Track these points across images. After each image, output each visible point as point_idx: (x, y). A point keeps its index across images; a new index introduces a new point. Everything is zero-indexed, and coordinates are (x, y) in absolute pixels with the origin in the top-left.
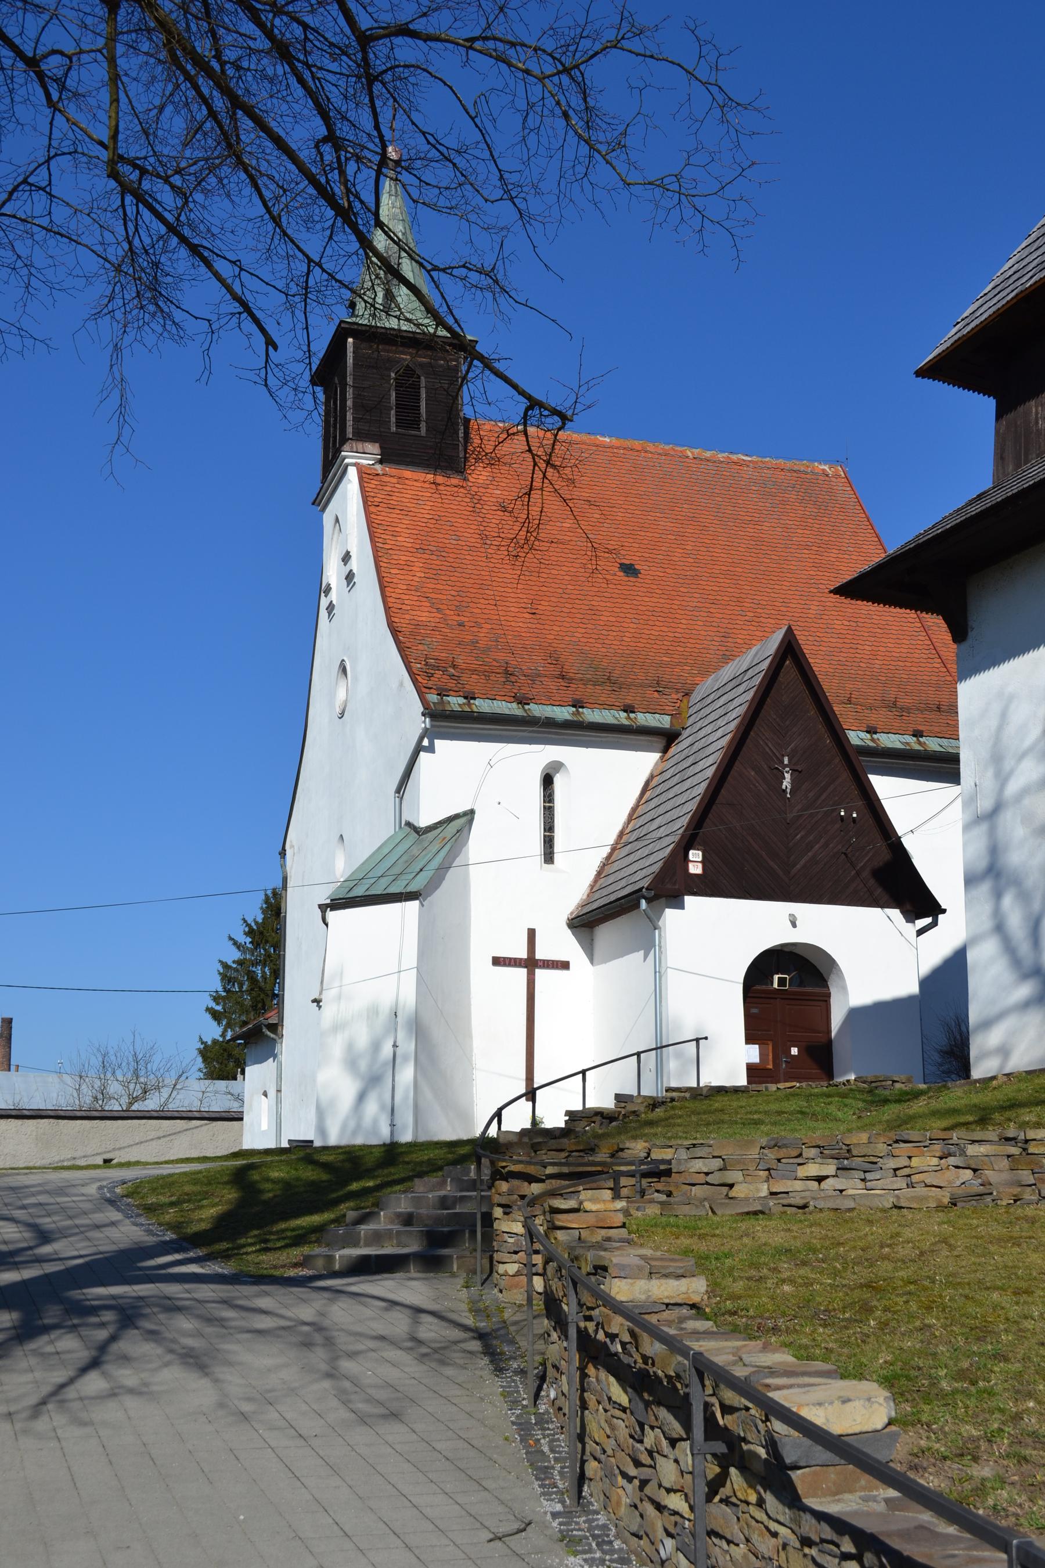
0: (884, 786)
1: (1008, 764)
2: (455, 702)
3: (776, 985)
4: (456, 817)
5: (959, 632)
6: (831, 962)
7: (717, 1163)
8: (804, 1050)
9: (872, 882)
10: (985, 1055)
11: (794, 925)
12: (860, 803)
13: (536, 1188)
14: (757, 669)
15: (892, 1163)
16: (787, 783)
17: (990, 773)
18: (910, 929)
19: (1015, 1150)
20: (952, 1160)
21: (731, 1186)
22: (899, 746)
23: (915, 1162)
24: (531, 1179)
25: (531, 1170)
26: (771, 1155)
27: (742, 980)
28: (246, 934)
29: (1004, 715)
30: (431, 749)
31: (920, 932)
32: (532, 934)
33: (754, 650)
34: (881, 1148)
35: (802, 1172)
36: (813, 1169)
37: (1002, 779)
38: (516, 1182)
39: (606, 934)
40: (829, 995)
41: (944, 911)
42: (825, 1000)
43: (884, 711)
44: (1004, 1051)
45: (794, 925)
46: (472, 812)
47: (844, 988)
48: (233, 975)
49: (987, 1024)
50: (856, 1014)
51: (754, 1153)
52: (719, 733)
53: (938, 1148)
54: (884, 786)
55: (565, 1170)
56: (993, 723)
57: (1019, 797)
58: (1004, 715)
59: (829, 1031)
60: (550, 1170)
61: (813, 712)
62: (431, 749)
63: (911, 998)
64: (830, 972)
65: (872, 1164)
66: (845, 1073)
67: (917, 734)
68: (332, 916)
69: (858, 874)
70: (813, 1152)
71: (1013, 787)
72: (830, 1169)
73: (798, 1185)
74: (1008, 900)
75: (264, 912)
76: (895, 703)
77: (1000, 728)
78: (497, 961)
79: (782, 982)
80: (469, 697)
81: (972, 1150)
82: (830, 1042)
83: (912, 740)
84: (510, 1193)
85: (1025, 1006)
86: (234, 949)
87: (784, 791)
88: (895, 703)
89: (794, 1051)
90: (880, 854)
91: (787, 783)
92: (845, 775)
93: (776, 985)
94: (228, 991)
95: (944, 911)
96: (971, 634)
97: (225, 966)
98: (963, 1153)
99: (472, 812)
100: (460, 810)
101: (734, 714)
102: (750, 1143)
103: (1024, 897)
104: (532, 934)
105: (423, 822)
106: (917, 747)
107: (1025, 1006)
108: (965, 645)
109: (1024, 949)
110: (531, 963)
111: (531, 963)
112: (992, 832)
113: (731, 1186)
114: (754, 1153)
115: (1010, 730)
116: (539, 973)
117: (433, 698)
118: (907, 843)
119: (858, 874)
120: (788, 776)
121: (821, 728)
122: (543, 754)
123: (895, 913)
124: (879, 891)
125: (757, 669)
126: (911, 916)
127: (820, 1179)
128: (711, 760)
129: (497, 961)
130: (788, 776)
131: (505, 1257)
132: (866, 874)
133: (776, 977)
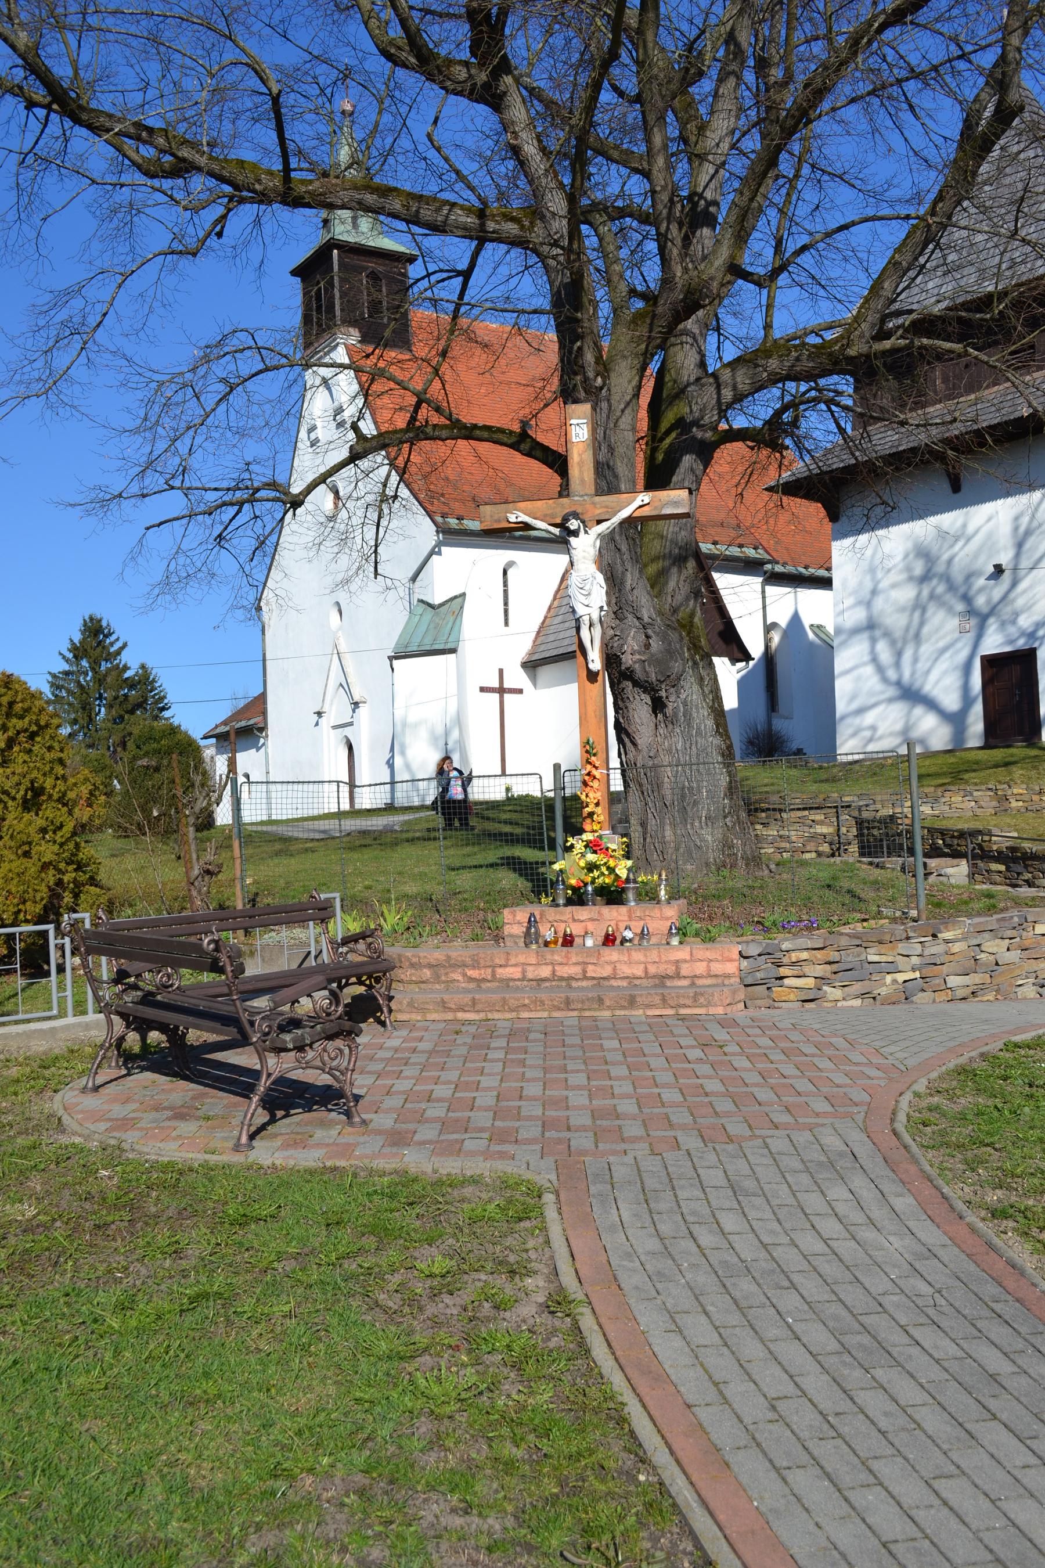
0: (723, 581)
2: (453, 522)
4: (456, 597)
5: (834, 516)
28: (70, 651)
30: (439, 553)
32: (501, 671)
39: (544, 672)
46: (463, 595)
48: (61, 683)
53: (962, 793)
62: (439, 553)
68: (395, 662)
75: (83, 633)
78: (482, 689)
80: (460, 518)
81: (975, 794)
83: (712, 547)
86: (63, 662)
94: (56, 696)
97: (54, 676)
99: (463, 595)
100: (457, 593)
104: (501, 671)
105: (437, 601)
108: (837, 525)
110: (501, 690)
111: (501, 690)
116: (506, 696)
117: (439, 519)
118: (737, 623)
122: (499, 557)
129: (482, 689)
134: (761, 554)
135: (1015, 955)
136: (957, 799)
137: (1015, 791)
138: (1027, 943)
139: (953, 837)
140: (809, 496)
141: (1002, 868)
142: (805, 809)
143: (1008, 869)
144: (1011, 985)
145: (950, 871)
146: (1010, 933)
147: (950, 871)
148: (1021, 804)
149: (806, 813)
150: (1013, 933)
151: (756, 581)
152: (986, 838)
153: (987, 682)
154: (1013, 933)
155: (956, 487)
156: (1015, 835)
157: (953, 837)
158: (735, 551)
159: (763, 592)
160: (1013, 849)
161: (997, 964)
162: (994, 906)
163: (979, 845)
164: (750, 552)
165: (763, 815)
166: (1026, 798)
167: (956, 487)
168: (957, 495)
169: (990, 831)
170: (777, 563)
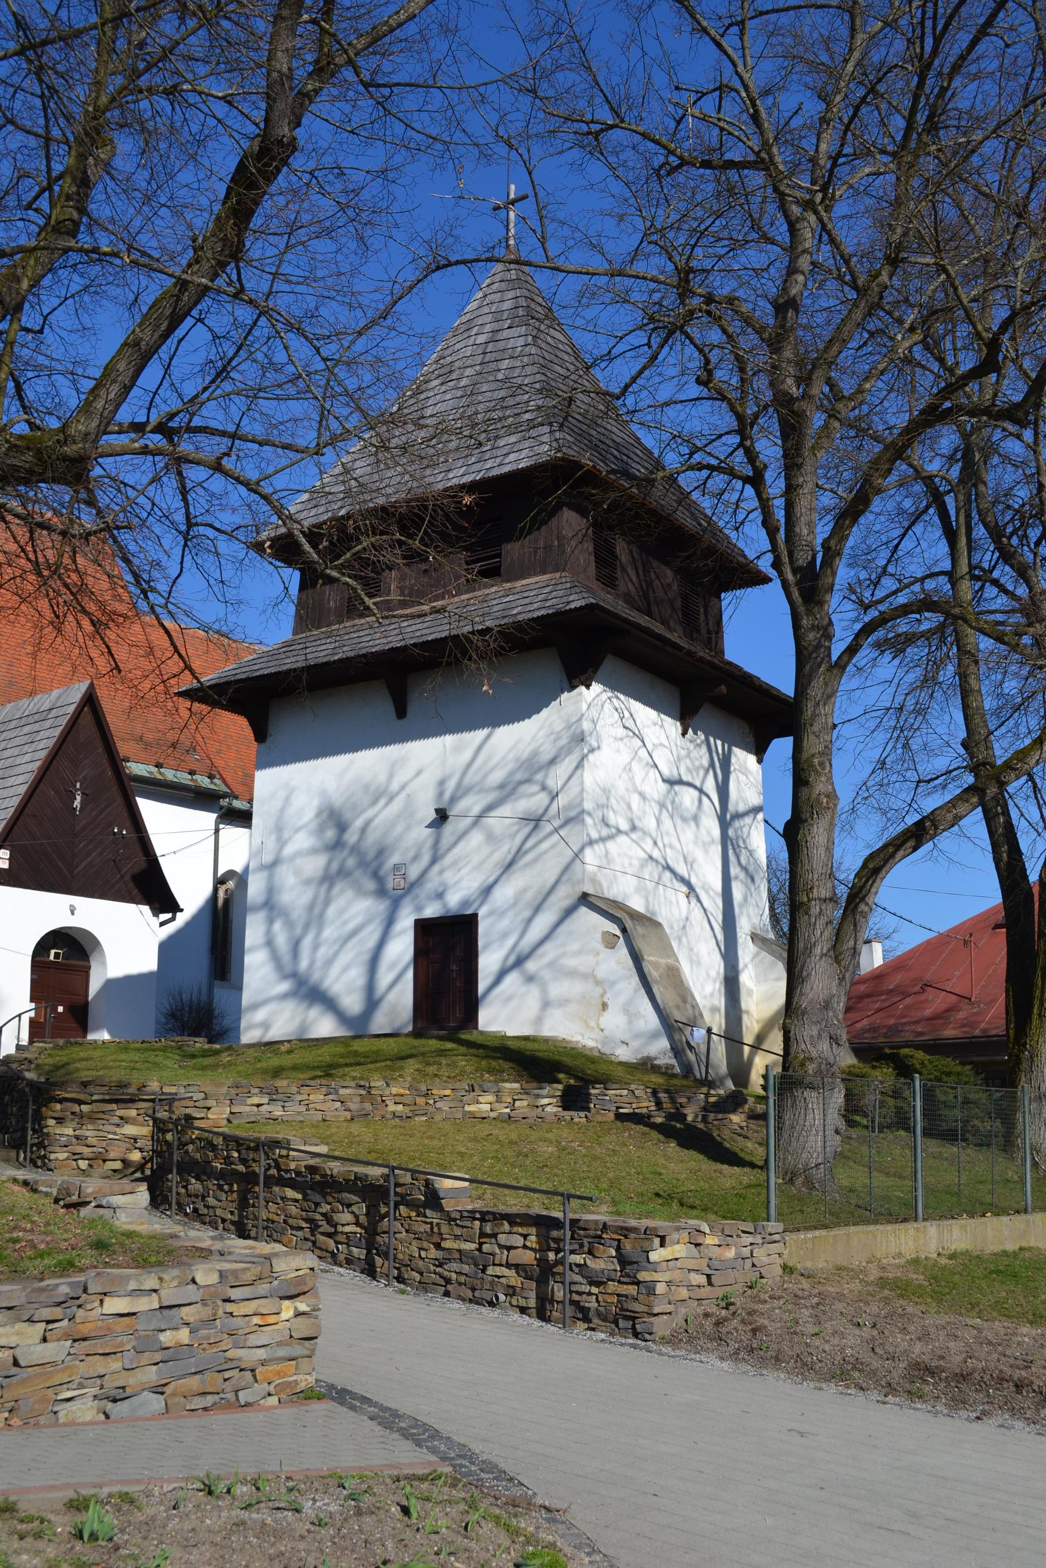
0: (150, 810)
1: (286, 834)
3: (52, 958)
5: (261, 735)
6: (95, 943)
7: (202, 1095)
8: (69, 1009)
9: (131, 884)
10: (251, 1027)
11: (73, 913)
12: (128, 823)
13: (85, 1108)
14: (62, 711)
15: (299, 1098)
16: (77, 803)
17: (273, 837)
18: (155, 922)
19: (363, 1092)
20: (331, 1097)
21: (209, 1109)
22: (147, 775)
23: (311, 1097)
24: (80, 1102)
25: (81, 1097)
26: (233, 1091)
27: (31, 953)
29: (287, 800)
31: (162, 924)
33: (55, 693)
34: (294, 1089)
35: (250, 1101)
36: (256, 1100)
37: (282, 843)
38: (69, 1104)
40: (89, 968)
41: (182, 910)
42: (86, 971)
43: (133, 744)
44: (266, 1025)
45: (73, 913)
47: (104, 964)
49: (255, 1007)
50: (112, 985)
51: (224, 1090)
52: (27, 758)
53: (324, 1090)
54: (150, 810)
55: (107, 1097)
56: (278, 804)
57: (293, 858)
58: (287, 800)
59: (87, 995)
60: (95, 1097)
61: (100, 750)
63: (150, 975)
64: (93, 950)
65: (289, 1098)
66: (98, 1028)
67: (159, 766)
69: (122, 877)
70: (257, 1090)
71: (288, 850)
72: (265, 1100)
73: (247, 1109)
74: (277, 926)
76: (141, 737)
77: (283, 809)
79: (57, 955)
81: (342, 1091)
82: (86, 1004)
83: (155, 770)
84: (62, 1110)
85: (284, 997)
87: (75, 809)
88: (141, 737)
89: (60, 1009)
90: (140, 862)
91: (77, 803)
92: (119, 801)
93: (52, 958)
95: (182, 910)
96: (269, 739)
98: (337, 1093)
101: (42, 745)
102: (221, 1084)
103: (289, 924)
106: (159, 777)
107: (284, 997)
108: (263, 746)
109: (286, 959)
112: (270, 878)
113: (209, 1109)
114: (224, 1090)
115: (291, 810)
119: (122, 877)
120: (78, 798)
121: (105, 761)
123: (146, 909)
124: (135, 891)
125: (62, 711)
126: (156, 911)
127: (258, 1106)
128: (21, 779)
130: (78, 798)
131: (58, 1149)
132: (127, 878)
133: (53, 952)
134: (218, 785)
135: (57, 1350)
136: (317, 1097)
137: (394, 1091)
138: (85, 1330)
139: (249, 1148)
140: (235, 706)
141: (299, 1196)
142: (110, 1101)
143: (305, 1199)
144: (44, 1400)
145: (117, 1200)
146: (47, 1313)
147: (117, 1200)
148: (400, 1107)
149: (114, 1106)
150: (57, 1313)
151: (209, 818)
152: (284, 1152)
153: (421, 952)
154: (57, 1313)
155: (401, 713)
156: (323, 1149)
157: (249, 1148)
158: (184, 778)
159: (217, 831)
160: (312, 1169)
161: (16, 1363)
162: (71, 1264)
163: (275, 1161)
164: (203, 781)
165: (58, 1106)
166: (408, 1100)
167: (401, 713)
168: (402, 722)
169: (288, 1142)
170: (236, 798)
